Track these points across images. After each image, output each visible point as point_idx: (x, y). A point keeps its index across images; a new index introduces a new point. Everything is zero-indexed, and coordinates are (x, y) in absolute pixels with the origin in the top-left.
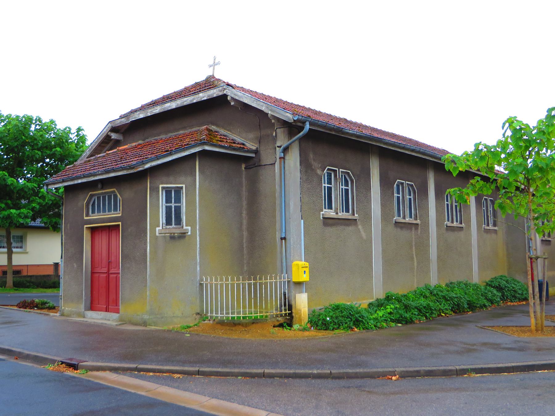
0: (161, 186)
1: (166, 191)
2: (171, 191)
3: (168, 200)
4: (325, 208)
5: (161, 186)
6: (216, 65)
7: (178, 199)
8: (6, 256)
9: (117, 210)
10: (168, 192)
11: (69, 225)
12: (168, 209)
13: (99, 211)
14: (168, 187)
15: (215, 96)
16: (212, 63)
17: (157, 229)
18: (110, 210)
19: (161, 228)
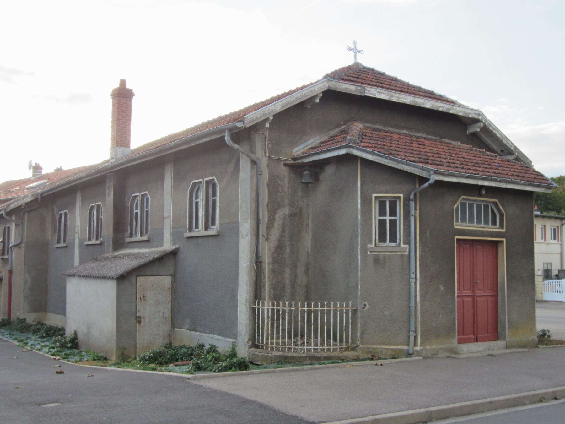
0: (374, 195)
1: (380, 202)
2: (385, 202)
3: (382, 212)
4: (558, 227)
5: (374, 195)
6: (355, 48)
7: (393, 212)
8: (559, 246)
9: (473, 222)
10: (382, 204)
11: (428, 232)
12: (382, 223)
13: (479, 222)
14: (380, 197)
15: (470, 116)
16: (359, 47)
17: (369, 245)
18: (479, 222)
19: (373, 245)
